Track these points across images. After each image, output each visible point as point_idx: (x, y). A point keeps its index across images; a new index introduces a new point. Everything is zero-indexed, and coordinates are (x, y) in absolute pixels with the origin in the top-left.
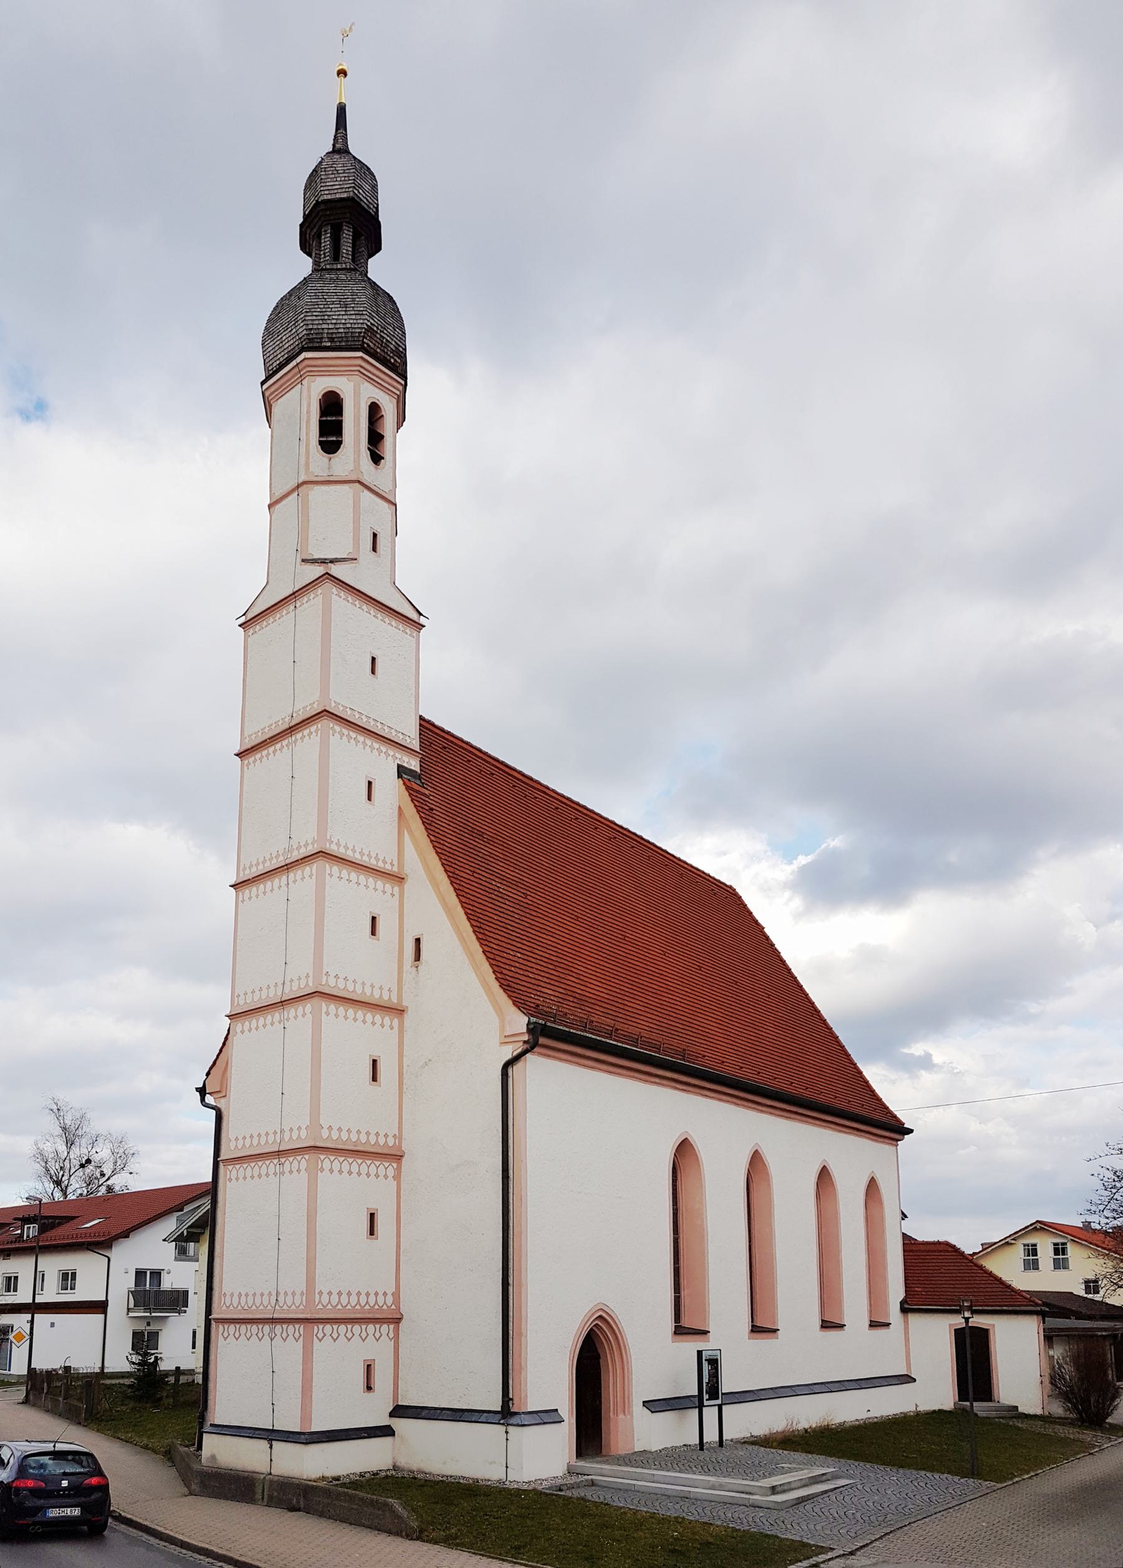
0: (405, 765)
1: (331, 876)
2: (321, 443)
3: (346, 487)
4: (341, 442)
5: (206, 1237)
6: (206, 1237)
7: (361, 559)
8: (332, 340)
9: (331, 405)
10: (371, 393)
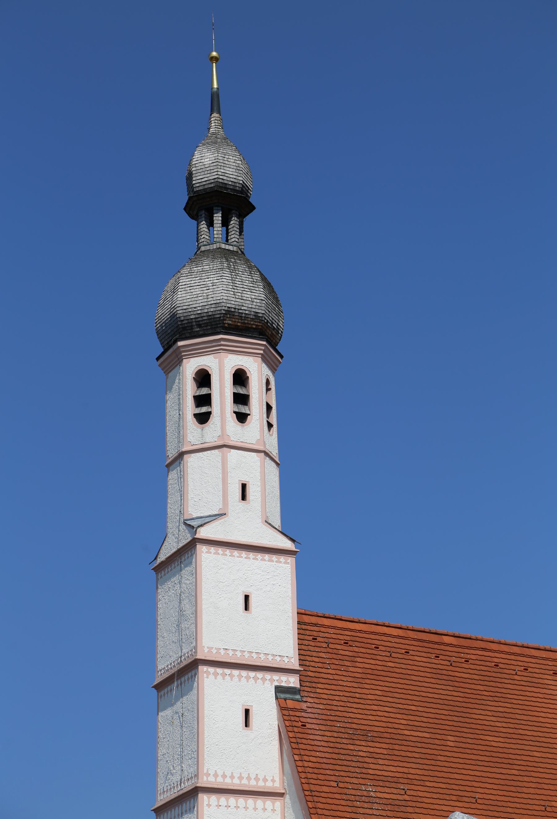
0: (283, 684)
1: (209, 805)
2: (196, 415)
3: (216, 452)
4: (210, 413)
5: (287, 544)
6: (287, 544)
7: (230, 512)
8: (199, 326)
9: (203, 378)
10: (233, 362)
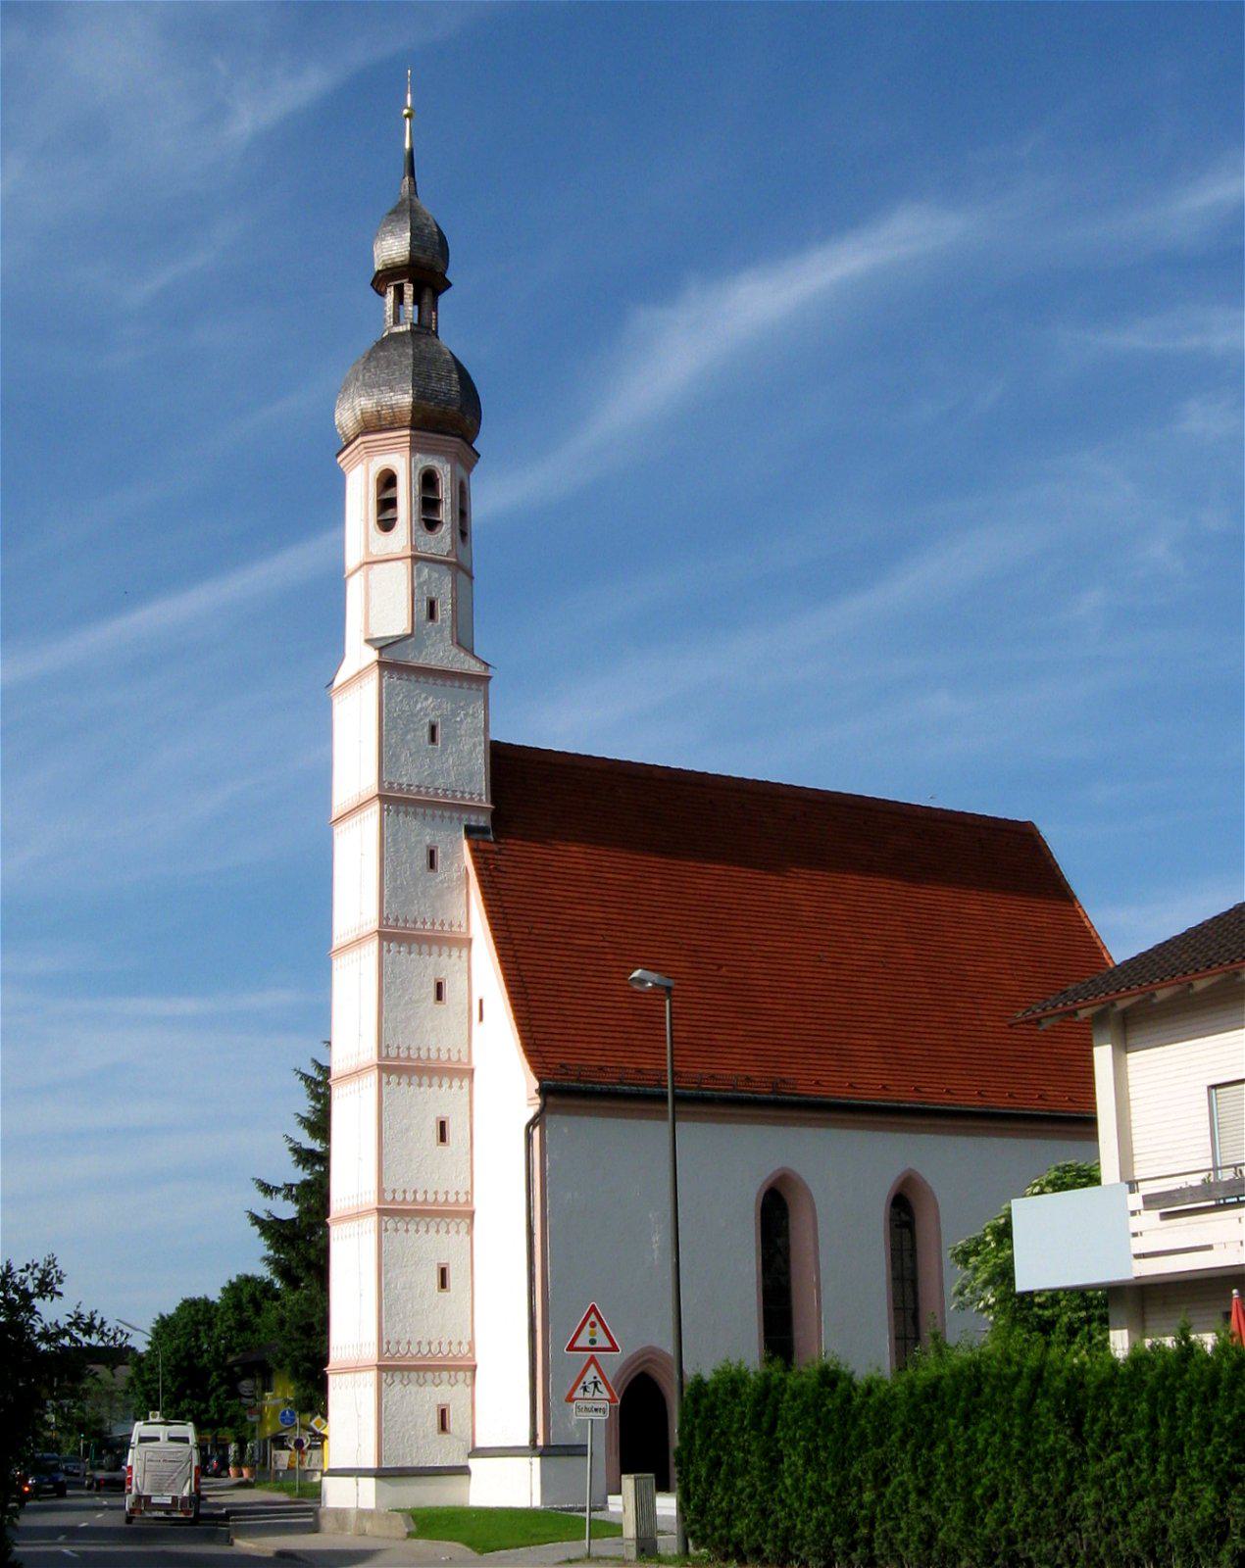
0: (473, 823)
